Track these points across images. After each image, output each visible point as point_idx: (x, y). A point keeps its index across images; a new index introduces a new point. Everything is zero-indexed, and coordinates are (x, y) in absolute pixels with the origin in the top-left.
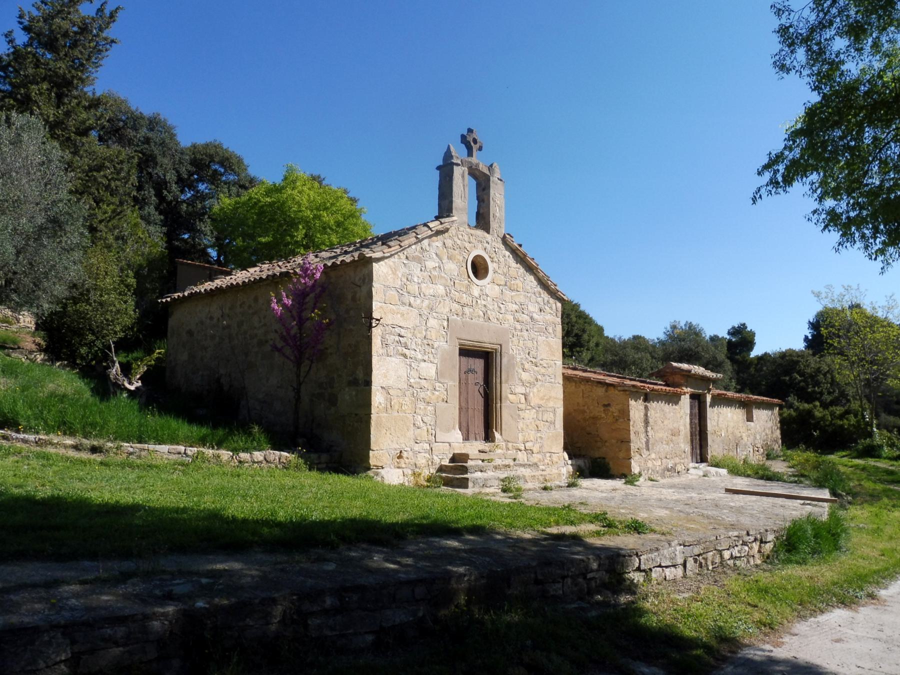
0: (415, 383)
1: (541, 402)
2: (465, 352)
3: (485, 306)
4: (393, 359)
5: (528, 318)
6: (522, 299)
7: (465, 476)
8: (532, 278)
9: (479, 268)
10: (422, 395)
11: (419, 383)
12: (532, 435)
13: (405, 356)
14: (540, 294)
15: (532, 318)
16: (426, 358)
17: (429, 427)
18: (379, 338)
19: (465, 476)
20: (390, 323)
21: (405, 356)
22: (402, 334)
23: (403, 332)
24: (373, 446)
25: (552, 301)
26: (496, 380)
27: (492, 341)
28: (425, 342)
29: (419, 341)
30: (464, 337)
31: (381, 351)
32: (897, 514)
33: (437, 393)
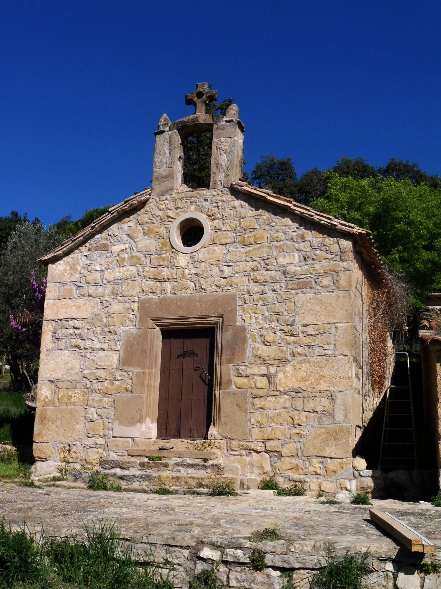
0: (90, 374)
1: (302, 385)
2: (169, 333)
3: (196, 274)
4: (64, 352)
5: (278, 275)
6: (264, 252)
7: (391, 415)
8: (288, 221)
9: (192, 233)
10: (97, 386)
11: (94, 373)
12: (281, 430)
13: (78, 347)
14: (303, 237)
15: (285, 273)
16: (105, 346)
17: (106, 420)
18: (50, 334)
19: (391, 415)
20: (62, 317)
21: (78, 347)
22: (76, 326)
23: (77, 323)
24: (35, 439)
25: (329, 241)
26: (217, 362)
27: (205, 314)
28: (107, 329)
29: (98, 330)
30: (161, 316)
31: (50, 346)
32: (1, 216)
33: (117, 383)
